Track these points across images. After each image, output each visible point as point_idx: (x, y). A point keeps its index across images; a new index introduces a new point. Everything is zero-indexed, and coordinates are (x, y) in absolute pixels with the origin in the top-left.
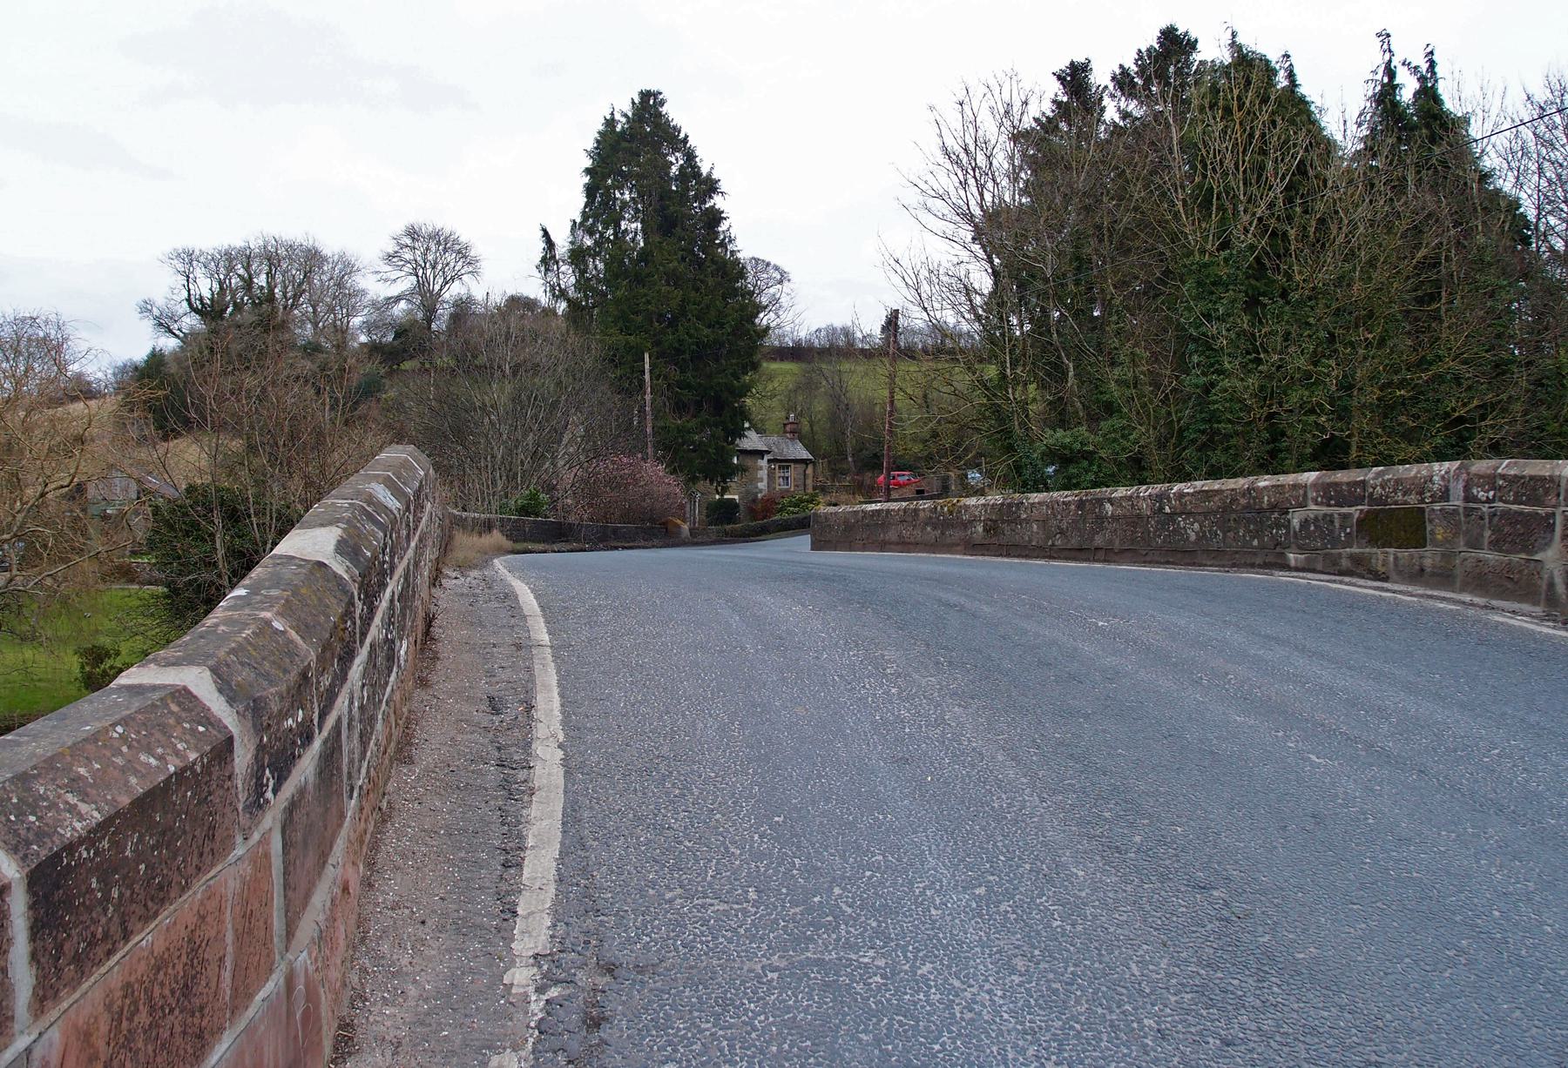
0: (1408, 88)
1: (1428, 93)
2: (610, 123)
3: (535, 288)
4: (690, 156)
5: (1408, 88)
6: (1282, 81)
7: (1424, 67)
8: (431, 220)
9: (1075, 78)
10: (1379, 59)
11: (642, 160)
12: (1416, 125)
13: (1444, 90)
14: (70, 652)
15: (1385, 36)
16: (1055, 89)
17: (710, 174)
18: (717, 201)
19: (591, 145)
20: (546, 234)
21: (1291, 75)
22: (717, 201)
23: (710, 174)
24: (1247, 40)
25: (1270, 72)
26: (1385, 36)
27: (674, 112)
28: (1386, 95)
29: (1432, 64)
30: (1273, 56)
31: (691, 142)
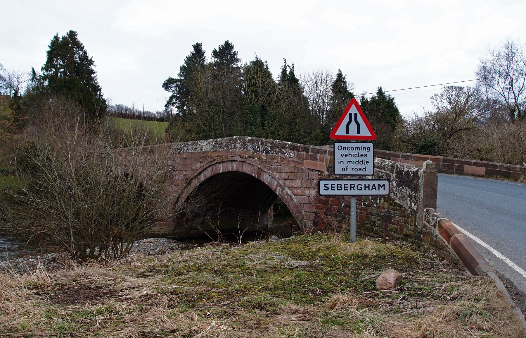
0: (288, 71)
1: (292, 73)
2: (56, 38)
3: (369, 100)
4: (85, 53)
5: (288, 71)
6: (265, 67)
7: (291, 67)
8: (163, 81)
9: (198, 47)
10: (283, 64)
11: (66, 52)
12: (289, 79)
13: (295, 73)
14: (283, 104)
15: (285, 59)
16: (192, 50)
17: (91, 59)
18: (92, 67)
19: (49, 44)
20: (33, 69)
21: (267, 66)
22: (92, 67)
23: (91, 59)
24: (259, 57)
25: (262, 65)
26: (285, 59)
27: (80, 38)
28: (284, 72)
29: (293, 67)
30: (263, 61)
31: (85, 48)
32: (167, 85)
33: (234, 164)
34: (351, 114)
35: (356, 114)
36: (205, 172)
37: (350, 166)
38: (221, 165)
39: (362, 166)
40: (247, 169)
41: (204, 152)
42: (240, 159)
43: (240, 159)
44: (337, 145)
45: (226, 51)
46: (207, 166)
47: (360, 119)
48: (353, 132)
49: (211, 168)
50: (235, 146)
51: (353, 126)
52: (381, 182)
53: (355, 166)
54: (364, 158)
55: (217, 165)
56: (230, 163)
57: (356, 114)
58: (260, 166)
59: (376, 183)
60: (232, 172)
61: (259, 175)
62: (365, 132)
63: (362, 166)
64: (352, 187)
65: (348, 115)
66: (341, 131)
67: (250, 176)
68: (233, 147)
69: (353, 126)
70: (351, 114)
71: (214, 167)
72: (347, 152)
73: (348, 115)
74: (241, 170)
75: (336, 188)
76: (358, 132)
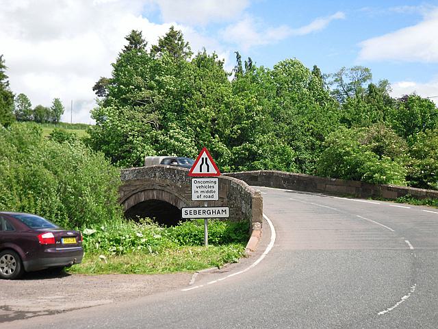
16: (127, 43)
32: (99, 88)
33: (155, 192)
34: (203, 158)
35: (206, 158)
36: (129, 200)
37: (203, 194)
38: (143, 193)
39: (211, 195)
40: (165, 197)
41: (128, 181)
42: (160, 188)
43: (160, 188)
44: (193, 180)
45: (171, 42)
46: (130, 194)
47: (209, 162)
48: (204, 171)
49: (134, 196)
50: (155, 174)
51: (204, 166)
52: (224, 209)
53: (206, 194)
54: (212, 189)
55: (139, 193)
56: (151, 191)
57: (206, 158)
58: (176, 194)
59: (220, 209)
60: (153, 200)
61: (176, 203)
62: (213, 170)
63: (211, 195)
64: (219, 212)
65: (201, 159)
66: (196, 171)
67: (168, 204)
68: (153, 175)
69: (204, 166)
70: (203, 158)
71: (136, 195)
72: (200, 185)
73: (201, 159)
74: (160, 198)
75: (193, 213)
76: (208, 171)
